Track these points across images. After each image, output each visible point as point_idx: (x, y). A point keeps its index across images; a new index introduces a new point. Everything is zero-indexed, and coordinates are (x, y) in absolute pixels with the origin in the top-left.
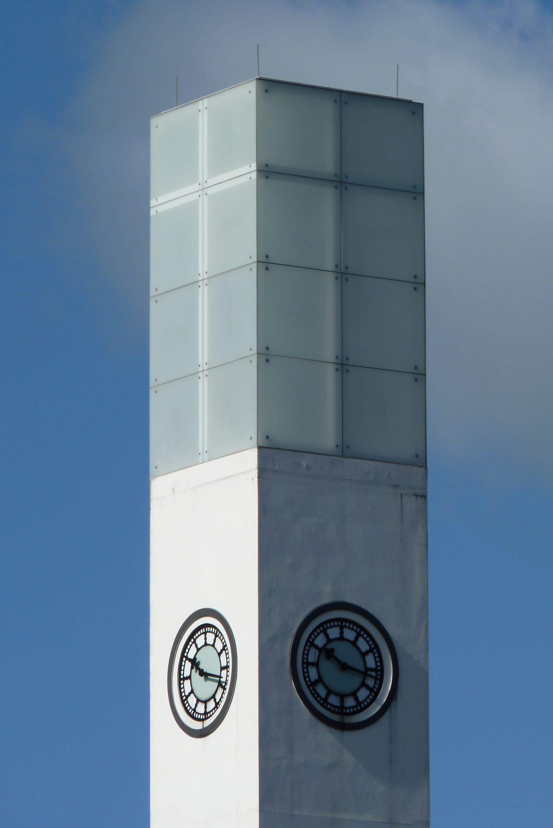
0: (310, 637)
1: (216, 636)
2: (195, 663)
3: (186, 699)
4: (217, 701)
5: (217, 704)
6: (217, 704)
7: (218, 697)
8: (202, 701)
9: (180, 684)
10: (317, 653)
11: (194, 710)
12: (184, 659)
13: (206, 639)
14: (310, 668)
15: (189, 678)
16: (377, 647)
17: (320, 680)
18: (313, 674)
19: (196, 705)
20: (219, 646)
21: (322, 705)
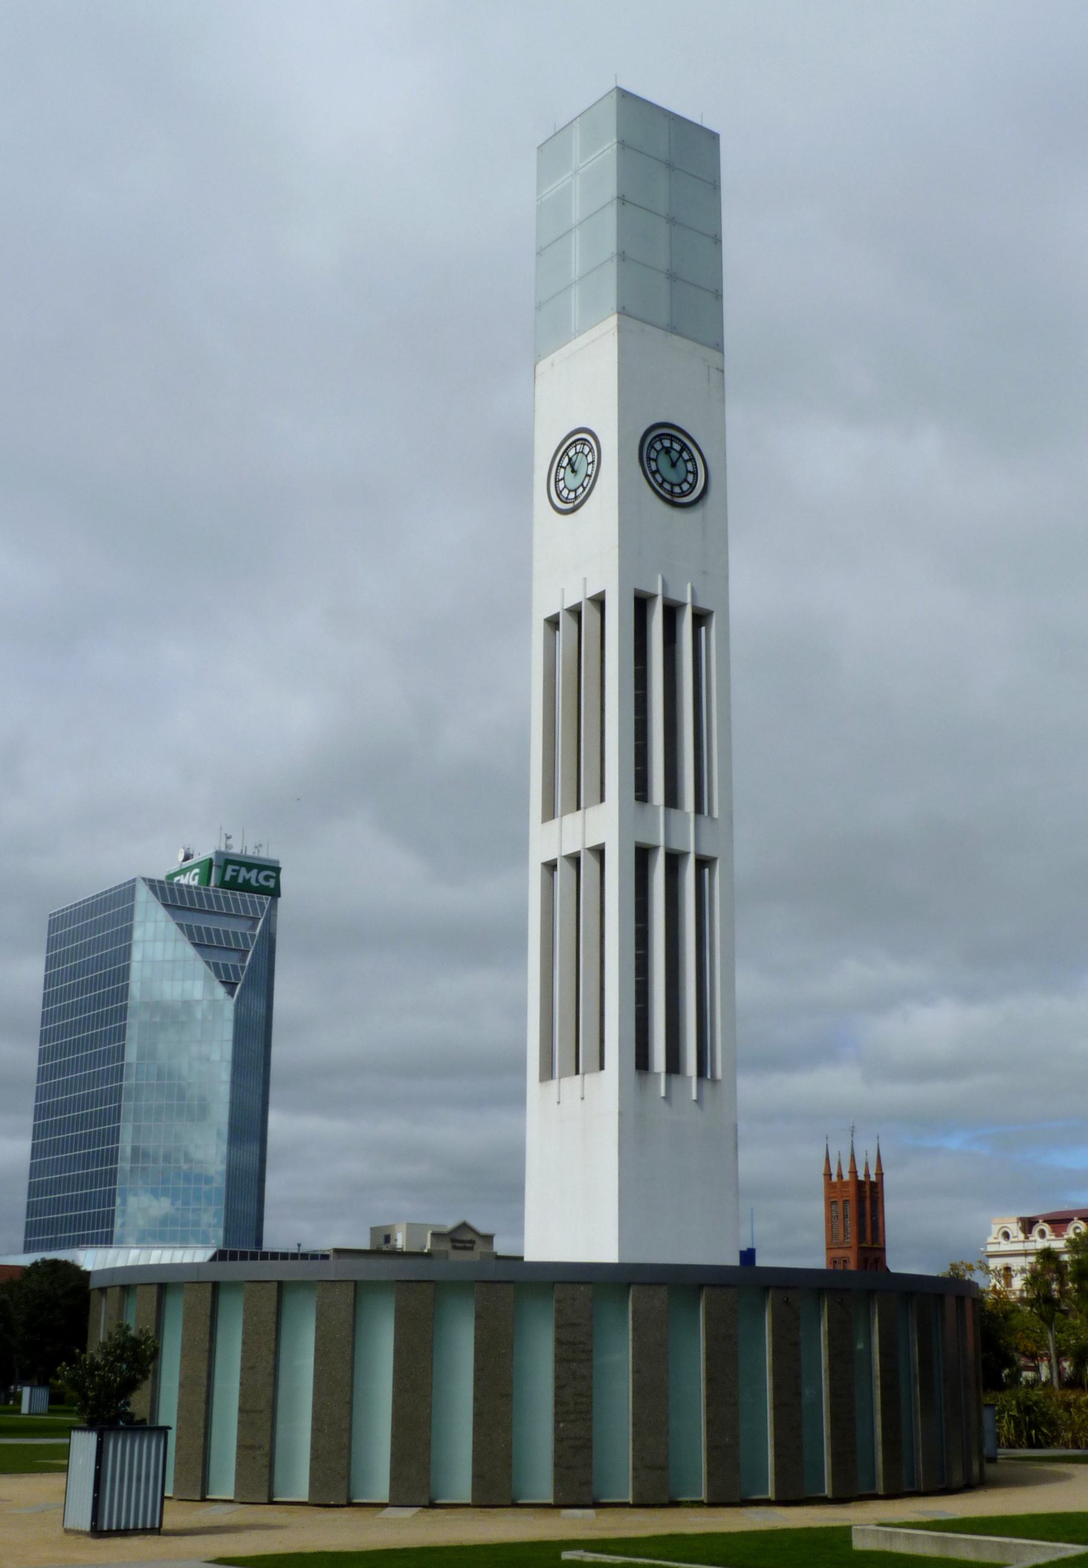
0: (651, 442)
1: (590, 451)
2: (571, 463)
3: (559, 481)
4: (577, 494)
5: (584, 489)
6: (576, 498)
7: (585, 484)
8: (567, 489)
9: (557, 469)
10: (656, 454)
11: (561, 492)
12: (566, 454)
13: (568, 494)
14: (651, 462)
15: (565, 468)
16: (693, 458)
17: (657, 471)
18: (654, 466)
19: (563, 489)
20: (590, 459)
21: (660, 487)
